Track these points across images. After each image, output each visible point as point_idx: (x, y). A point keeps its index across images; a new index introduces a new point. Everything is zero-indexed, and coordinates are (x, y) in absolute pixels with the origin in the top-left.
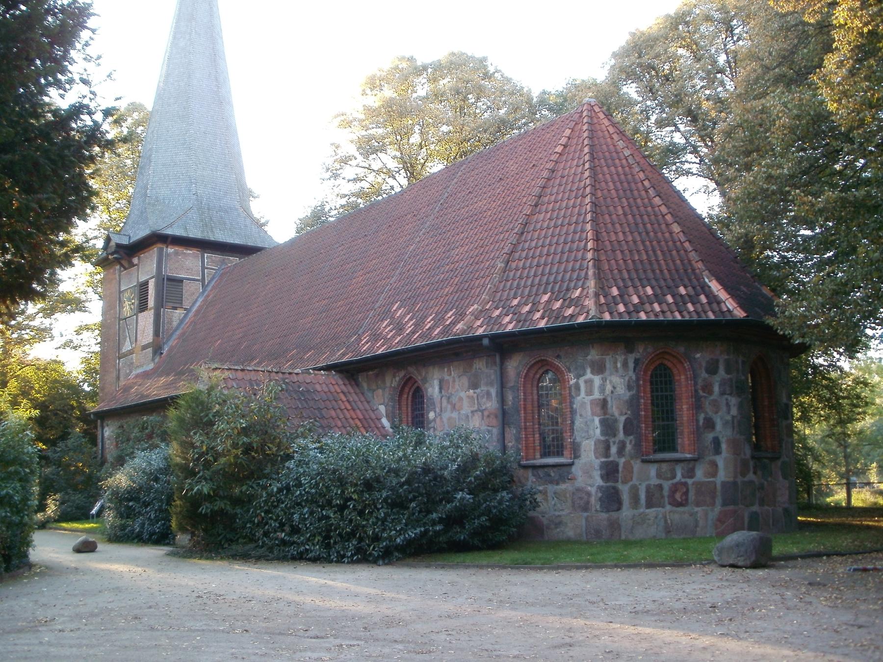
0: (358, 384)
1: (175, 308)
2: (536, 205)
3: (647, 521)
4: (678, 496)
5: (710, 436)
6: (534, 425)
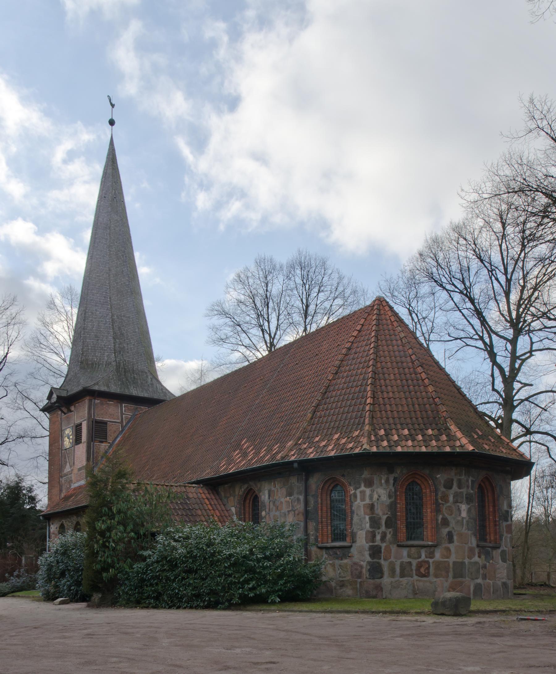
0: (218, 494)
1: (102, 442)
2: (336, 373)
3: (401, 586)
4: (422, 570)
5: (445, 531)
6: (327, 520)
